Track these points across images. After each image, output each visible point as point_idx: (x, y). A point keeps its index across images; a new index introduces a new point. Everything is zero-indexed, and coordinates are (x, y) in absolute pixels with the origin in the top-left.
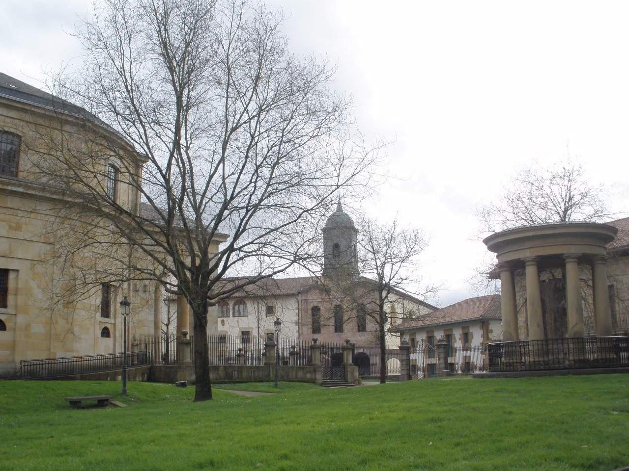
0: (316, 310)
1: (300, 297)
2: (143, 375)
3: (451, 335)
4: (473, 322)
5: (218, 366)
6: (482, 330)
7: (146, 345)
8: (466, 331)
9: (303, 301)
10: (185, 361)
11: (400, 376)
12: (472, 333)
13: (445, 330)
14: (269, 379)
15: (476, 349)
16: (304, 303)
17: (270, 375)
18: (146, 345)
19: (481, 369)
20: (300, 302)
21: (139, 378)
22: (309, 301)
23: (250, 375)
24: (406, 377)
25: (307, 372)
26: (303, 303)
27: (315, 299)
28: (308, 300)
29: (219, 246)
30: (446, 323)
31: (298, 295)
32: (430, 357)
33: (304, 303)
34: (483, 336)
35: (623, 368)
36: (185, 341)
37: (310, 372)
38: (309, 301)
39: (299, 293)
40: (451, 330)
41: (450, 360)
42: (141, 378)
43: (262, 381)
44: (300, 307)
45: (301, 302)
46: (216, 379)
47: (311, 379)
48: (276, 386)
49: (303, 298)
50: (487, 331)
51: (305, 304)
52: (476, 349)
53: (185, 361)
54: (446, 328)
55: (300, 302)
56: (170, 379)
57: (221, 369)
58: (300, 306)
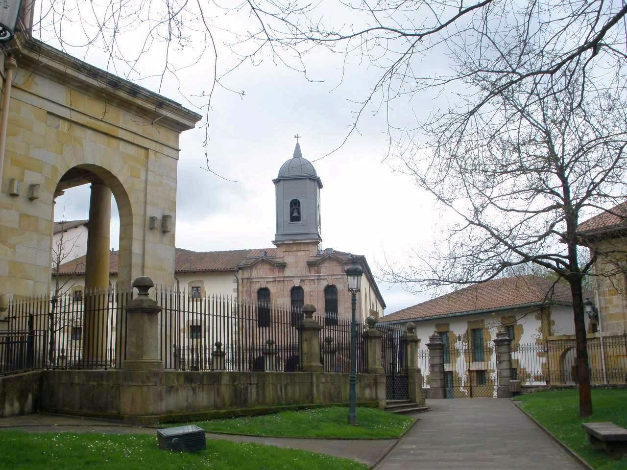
0: (264, 293)
1: (240, 275)
2: (22, 398)
3: (480, 330)
4: (525, 310)
5: (220, 373)
6: (540, 321)
7: (31, 317)
8: (443, 329)
9: (245, 281)
10: (147, 358)
11: (428, 389)
12: (521, 326)
13: (469, 322)
14: (312, 402)
15: (528, 349)
16: (246, 284)
17: (311, 395)
18: (31, 317)
19: (537, 378)
20: (240, 281)
21: (12, 405)
22: (254, 280)
23: (279, 393)
24: (441, 392)
25: (366, 386)
26: (245, 283)
27: (262, 276)
28: (252, 279)
29: (180, 135)
30: (466, 313)
31: (238, 271)
32: (475, 360)
33: (246, 284)
34: (541, 330)
35: (17, 375)
36: (145, 305)
37: (369, 386)
38: (254, 280)
39: (240, 269)
40: (448, 325)
41: (448, 367)
42: (17, 405)
43: (302, 408)
44: (240, 289)
45: (243, 282)
46: (216, 407)
47: (371, 399)
48: (351, 420)
49: (246, 276)
50: (549, 323)
51: (248, 284)
52: (528, 349)
53: (147, 358)
54: (472, 320)
55: (240, 281)
56: (103, 411)
57: (225, 380)
58: (240, 287)
